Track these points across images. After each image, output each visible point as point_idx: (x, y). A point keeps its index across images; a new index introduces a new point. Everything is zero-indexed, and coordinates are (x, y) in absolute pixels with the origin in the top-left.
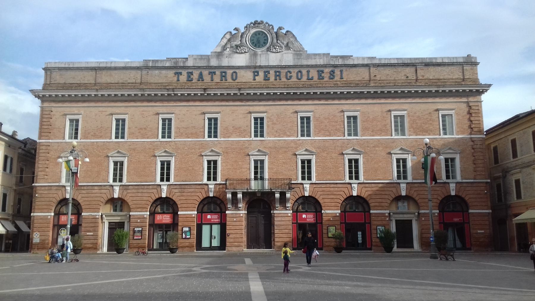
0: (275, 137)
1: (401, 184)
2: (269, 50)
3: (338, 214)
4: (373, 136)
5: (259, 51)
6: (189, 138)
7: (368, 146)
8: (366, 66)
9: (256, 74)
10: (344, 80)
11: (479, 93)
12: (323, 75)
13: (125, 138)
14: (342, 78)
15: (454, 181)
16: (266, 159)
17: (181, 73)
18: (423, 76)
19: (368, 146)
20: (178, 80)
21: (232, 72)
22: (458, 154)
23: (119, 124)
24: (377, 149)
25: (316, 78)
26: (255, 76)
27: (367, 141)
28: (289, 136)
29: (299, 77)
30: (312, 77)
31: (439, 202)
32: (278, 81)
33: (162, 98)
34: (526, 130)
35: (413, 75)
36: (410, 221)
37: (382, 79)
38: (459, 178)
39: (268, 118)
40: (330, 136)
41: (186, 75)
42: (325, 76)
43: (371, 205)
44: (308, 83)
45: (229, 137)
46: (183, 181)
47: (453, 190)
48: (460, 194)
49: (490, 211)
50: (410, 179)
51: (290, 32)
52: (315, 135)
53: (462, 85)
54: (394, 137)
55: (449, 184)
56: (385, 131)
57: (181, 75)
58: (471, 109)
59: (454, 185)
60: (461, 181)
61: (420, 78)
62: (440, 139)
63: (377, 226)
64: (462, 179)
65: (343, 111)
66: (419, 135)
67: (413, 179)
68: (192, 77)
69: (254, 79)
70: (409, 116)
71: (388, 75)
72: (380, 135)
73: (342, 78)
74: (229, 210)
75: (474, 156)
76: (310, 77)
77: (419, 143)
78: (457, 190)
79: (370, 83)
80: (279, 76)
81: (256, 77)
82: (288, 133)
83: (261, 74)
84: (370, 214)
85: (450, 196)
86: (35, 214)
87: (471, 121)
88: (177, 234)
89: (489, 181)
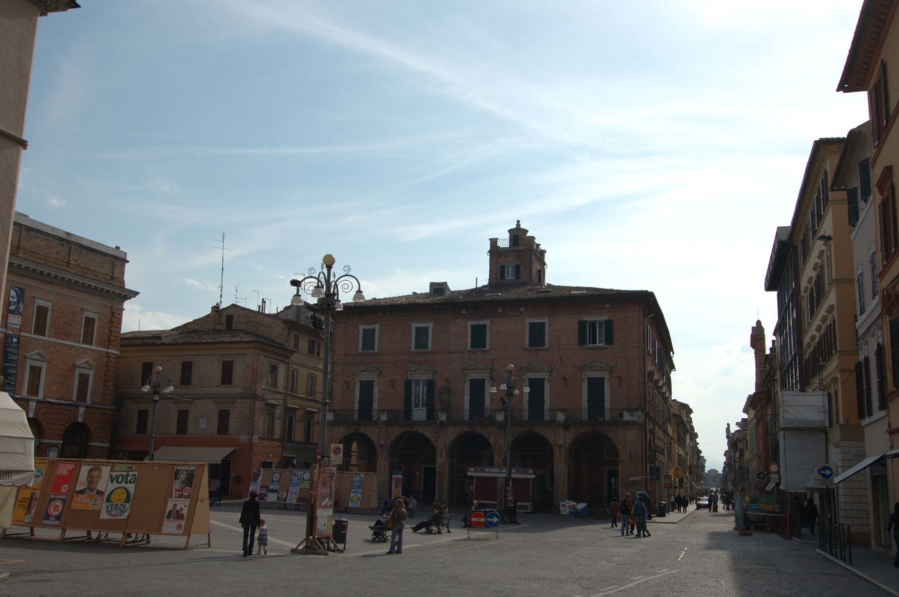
1: (30, 402)
8: (18, 225)
11: (126, 298)
16: (44, 366)
22: (45, 363)
35: (65, 256)
49: (108, 445)
50: (41, 397)
52: (50, 336)
53: (110, 283)
58: (113, 316)
61: (72, 262)
62: (78, 348)
65: (82, 309)
66: (60, 338)
70: (53, 310)
71: (39, 247)
75: (106, 376)
77: (57, 349)
79: (19, 252)
84: (63, 440)
85: (77, 423)
86: (93, 444)
87: (111, 332)
88: (326, 488)
89: (114, 408)
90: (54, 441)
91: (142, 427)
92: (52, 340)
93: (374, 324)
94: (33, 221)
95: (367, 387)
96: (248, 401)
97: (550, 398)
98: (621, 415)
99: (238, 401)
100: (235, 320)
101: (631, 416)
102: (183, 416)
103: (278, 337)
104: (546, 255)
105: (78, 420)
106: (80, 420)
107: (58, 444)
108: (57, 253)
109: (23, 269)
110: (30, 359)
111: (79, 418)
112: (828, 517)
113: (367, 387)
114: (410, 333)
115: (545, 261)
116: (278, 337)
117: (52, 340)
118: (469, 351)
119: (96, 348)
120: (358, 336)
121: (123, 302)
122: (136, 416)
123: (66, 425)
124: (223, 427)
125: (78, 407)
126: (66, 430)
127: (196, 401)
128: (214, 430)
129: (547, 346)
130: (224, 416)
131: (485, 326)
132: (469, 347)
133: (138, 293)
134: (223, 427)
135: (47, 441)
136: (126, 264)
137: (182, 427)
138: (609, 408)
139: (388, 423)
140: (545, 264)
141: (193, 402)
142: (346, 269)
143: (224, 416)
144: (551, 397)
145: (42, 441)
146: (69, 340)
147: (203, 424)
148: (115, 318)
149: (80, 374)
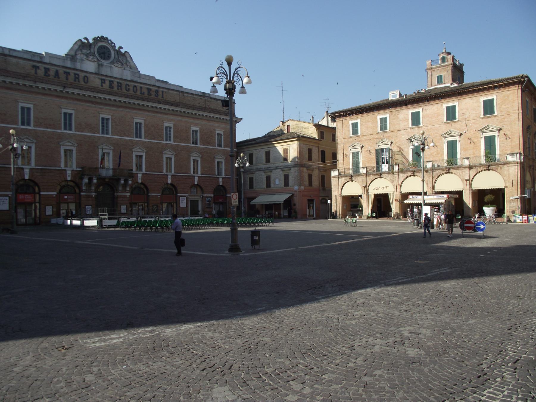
0: (118, 136)
2: (112, 63)
3: (54, 196)
4: (180, 143)
5: (104, 62)
6: (47, 128)
7: (177, 150)
9: (103, 81)
10: (164, 99)
12: (151, 92)
13: (252, 153)
14: (163, 97)
15: (222, 177)
17: (38, 67)
18: (208, 106)
19: (177, 150)
20: (36, 73)
21: (84, 75)
23: (104, 122)
24: (183, 152)
25: (146, 93)
26: (102, 83)
27: (177, 146)
28: (127, 136)
29: (135, 91)
30: (144, 93)
31: (213, 189)
32: (120, 90)
33: (199, 117)
34: (261, 150)
36: (198, 201)
37: (186, 103)
38: (33, 165)
39: (112, 119)
40: (154, 139)
41: (43, 70)
42: (152, 93)
43: (179, 190)
44: (141, 97)
45: (82, 132)
46: (43, 166)
47: (69, 176)
48: (224, 185)
51: (128, 52)
52: (200, 145)
54: (101, 135)
55: (24, 170)
56: (93, 130)
57: (151, 91)
59: (222, 179)
60: (145, 173)
63: (85, 206)
64: (146, 172)
67: (201, 174)
68: (49, 73)
69: (102, 86)
71: (190, 101)
72: (184, 143)
73: (163, 97)
74: (83, 192)
76: (142, 92)
78: (223, 182)
80: (121, 86)
81: (103, 85)
82: (127, 134)
83: (107, 83)
90: (209, 195)
91: (251, 186)
92: (202, 146)
93: (357, 119)
94: (185, 89)
95: (356, 155)
96: (296, 168)
97: (461, 152)
98: (507, 158)
99: (292, 169)
100: (291, 127)
101: (512, 157)
102: (268, 179)
103: (312, 134)
104: (464, 67)
105: (67, 179)
106: (221, 184)
107: (158, 196)
108: (199, 103)
109: (14, 84)
110: (135, 151)
111: (139, 180)
112: (125, 368)
113: (356, 155)
114: (377, 122)
115: (464, 71)
116: (312, 134)
117: (202, 146)
118: (411, 128)
119: (224, 149)
120: (349, 127)
121: (235, 124)
122: (248, 180)
123: (214, 187)
124: (286, 184)
125: (218, 178)
126: (215, 189)
127: (273, 171)
128: (283, 185)
129: (457, 120)
130: (286, 177)
131: (419, 112)
132: (410, 126)
133: (242, 119)
134: (286, 184)
135: (206, 195)
136: (235, 105)
137: (268, 185)
138: (499, 154)
139: (366, 175)
140: (464, 72)
141: (272, 172)
142: (239, 63)
143: (286, 177)
144: (461, 150)
145: (204, 195)
146: (210, 146)
147: (277, 182)
148: (232, 133)
149: (65, 150)
